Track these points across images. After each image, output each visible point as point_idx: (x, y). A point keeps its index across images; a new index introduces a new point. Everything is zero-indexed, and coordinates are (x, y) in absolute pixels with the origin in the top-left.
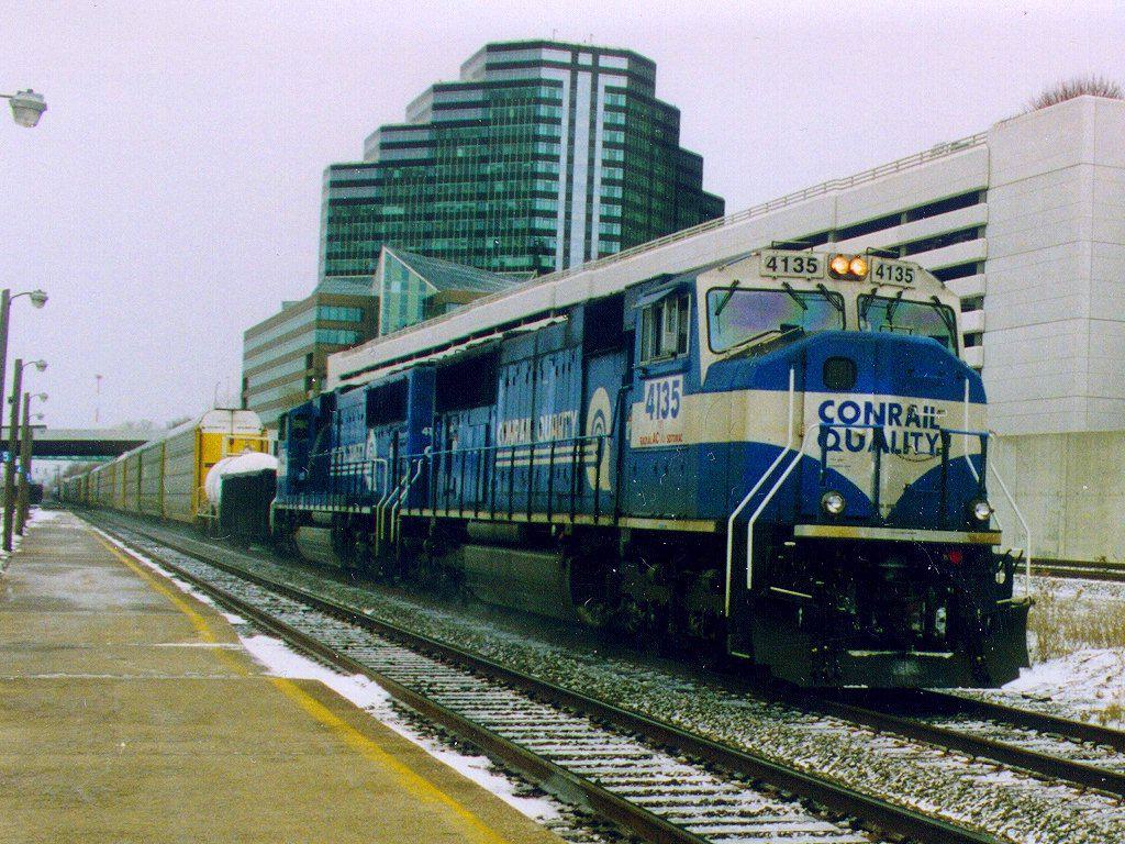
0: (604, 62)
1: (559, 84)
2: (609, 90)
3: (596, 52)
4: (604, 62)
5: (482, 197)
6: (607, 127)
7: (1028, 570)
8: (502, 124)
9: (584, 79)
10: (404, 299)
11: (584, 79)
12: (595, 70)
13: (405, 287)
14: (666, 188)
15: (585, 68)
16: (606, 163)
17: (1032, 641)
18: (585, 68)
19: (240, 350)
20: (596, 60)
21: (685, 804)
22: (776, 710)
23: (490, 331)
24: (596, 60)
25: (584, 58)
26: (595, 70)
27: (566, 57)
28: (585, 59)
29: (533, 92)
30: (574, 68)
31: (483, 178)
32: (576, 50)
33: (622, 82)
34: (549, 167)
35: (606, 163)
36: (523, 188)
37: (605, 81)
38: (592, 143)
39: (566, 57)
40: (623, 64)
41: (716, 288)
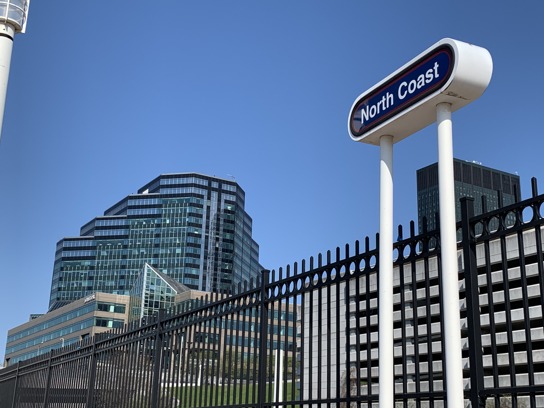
1: (202, 197)
2: (226, 202)
4: (225, 187)
7: (8, 5)
9: (214, 195)
11: (214, 195)
12: (220, 191)
15: (214, 189)
18: (214, 189)
19: (53, 259)
20: (220, 186)
21: (187, 185)
24: (220, 186)
26: (220, 191)
27: (205, 183)
28: (215, 185)
29: (194, 261)
30: (209, 189)
34: (194, 261)
36: (178, 242)
37: (224, 197)
38: (208, 217)
39: (205, 183)
40: (233, 189)
41: (66, 240)
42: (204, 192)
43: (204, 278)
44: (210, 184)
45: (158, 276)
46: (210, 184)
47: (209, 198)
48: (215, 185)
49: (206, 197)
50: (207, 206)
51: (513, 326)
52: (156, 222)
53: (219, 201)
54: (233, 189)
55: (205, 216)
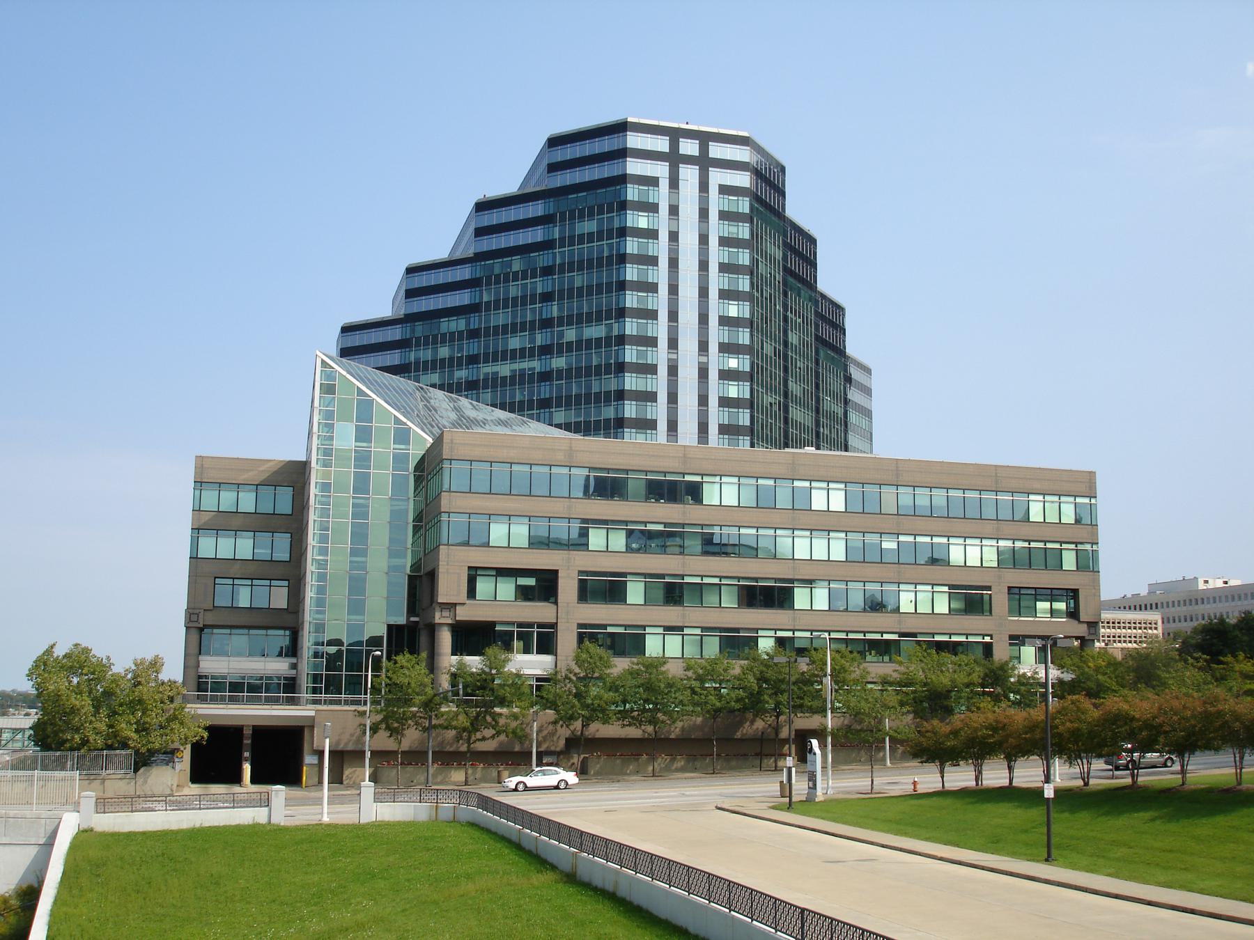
0: (717, 151)
1: (653, 182)
2: (725, 190)
3: (705, 138)
4: (717, 151)
5: (546, 350)
6: (652, 369)
8: (572, 244)
9: (689, 174)
10: (363, 459)
11: (689, 174)
12: (704, 163)
13: (363, 434)
14: (801, 365)
15: (689, 160)
16: (725, 295)
17: (453, 396)
18: (689, 160)
20: (704, 149)
22: (680, 763)
23: (512, 623)
24: (704, 149)
25: (690, 149)
26: (704, 163)
28: (689, 147)
30: (674, 159)
31: (547, 323)
32: (675, 135)
33: (743, 179)
35: (651, 397)
37: (718, 177)
38: (673, 316)
40: (741, 154)
42: (660, 170)
43: (674, 237)
44: (674, 145)
45: (397, 420)
46: (674, 145)
47: (674, 183)
48: (689, 147)
49: (664, 184)
50: (670, 232)
51: (583, 585)
52: (538, 343)
53: (704, 186)
54: (741, 154)
55: (662, 397)
